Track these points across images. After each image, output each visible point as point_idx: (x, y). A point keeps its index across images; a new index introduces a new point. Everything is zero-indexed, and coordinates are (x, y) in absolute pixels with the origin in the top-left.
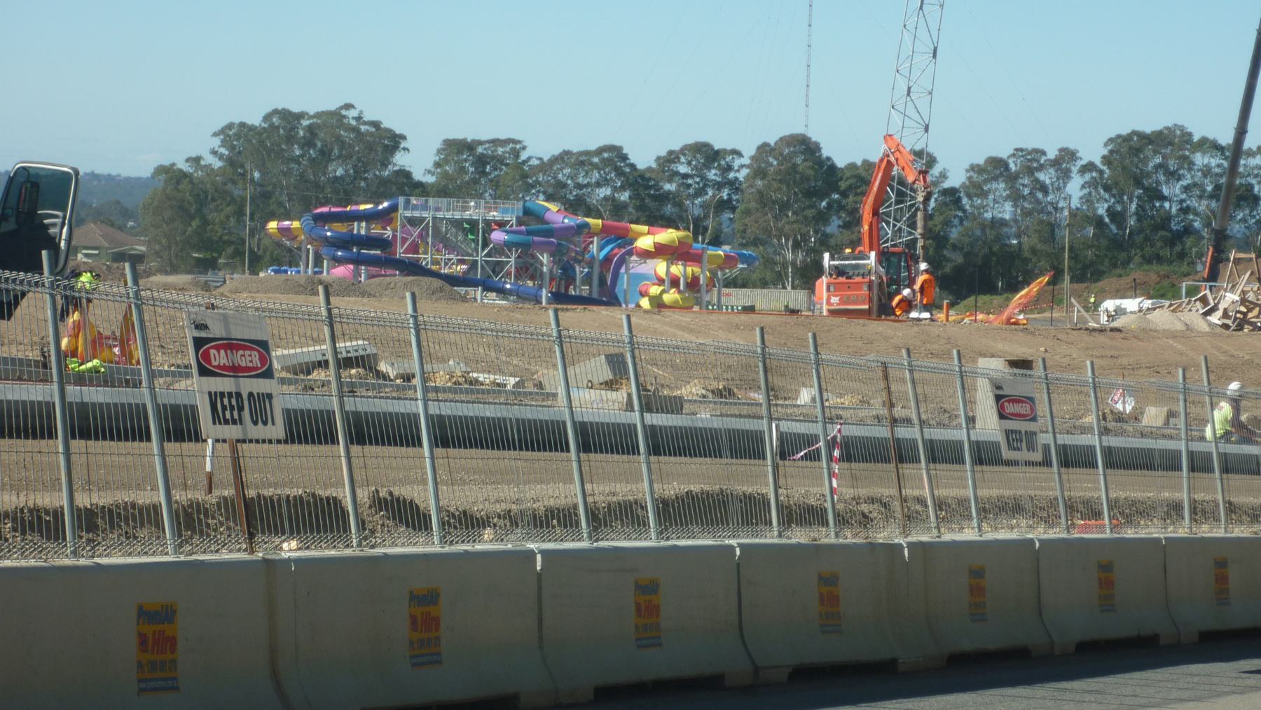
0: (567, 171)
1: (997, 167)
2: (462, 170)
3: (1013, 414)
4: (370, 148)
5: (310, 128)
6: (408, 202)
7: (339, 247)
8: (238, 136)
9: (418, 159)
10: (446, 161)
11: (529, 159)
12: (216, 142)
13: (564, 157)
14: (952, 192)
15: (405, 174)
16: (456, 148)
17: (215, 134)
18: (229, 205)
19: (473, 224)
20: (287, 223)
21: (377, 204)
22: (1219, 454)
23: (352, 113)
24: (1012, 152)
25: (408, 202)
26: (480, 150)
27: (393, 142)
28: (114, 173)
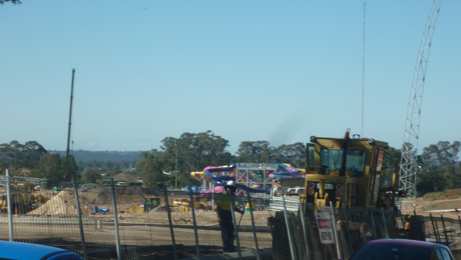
0: (284, 151)
1: (434, 148)
2: (248, 152)
3: (323, 226)
4: (217, 145)
5: (197, 139)
6: (239, 165)
7: (219, 181)
8: (170, 142)
9: (233, 149)
10: (243, 149)
11: (271, 147)
12: (162, 144)
13: (283, 147)
14: (419, 157)
15: (228, 154)
16: (246, 144)
17: (162, 141)
18: (169, 165)
19: (261, 172)
20: (198, 172)
21: (229, 165)
22: (121, 246)
23: (211, 134)
24: (438, 143)
25: (239, 165)
26: (254, 145)
27: (225, 143)
28: (88, 150)
